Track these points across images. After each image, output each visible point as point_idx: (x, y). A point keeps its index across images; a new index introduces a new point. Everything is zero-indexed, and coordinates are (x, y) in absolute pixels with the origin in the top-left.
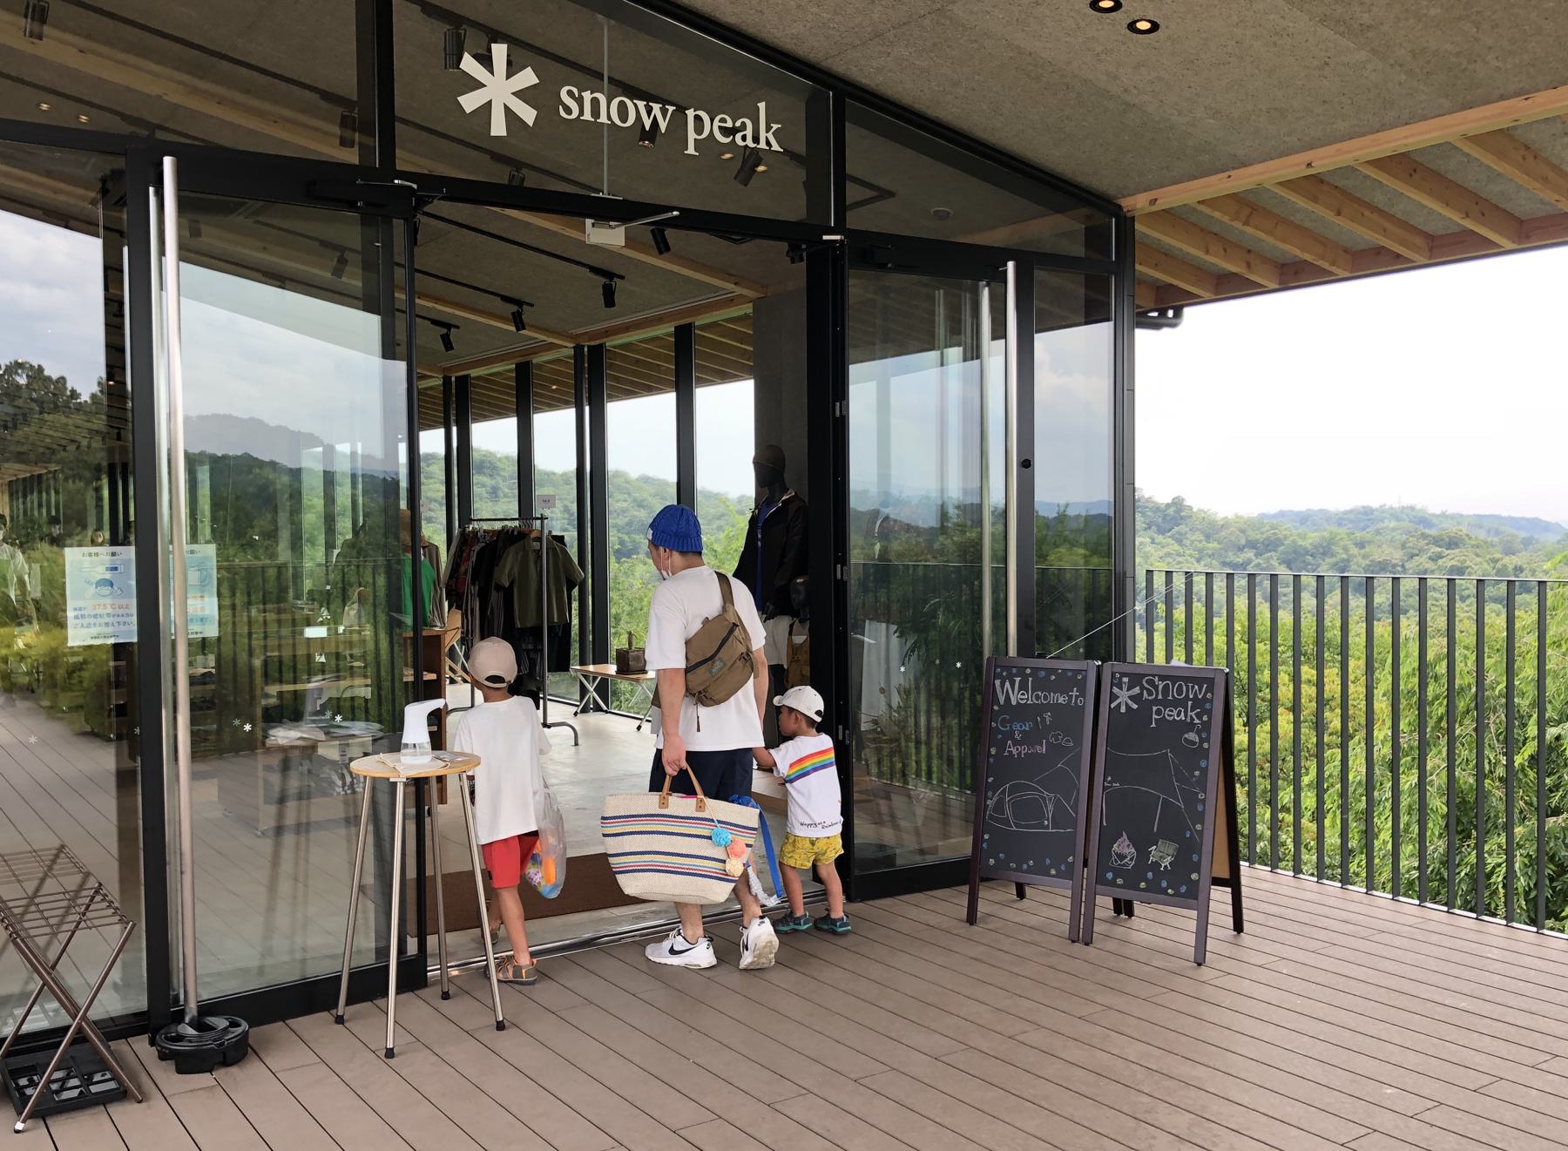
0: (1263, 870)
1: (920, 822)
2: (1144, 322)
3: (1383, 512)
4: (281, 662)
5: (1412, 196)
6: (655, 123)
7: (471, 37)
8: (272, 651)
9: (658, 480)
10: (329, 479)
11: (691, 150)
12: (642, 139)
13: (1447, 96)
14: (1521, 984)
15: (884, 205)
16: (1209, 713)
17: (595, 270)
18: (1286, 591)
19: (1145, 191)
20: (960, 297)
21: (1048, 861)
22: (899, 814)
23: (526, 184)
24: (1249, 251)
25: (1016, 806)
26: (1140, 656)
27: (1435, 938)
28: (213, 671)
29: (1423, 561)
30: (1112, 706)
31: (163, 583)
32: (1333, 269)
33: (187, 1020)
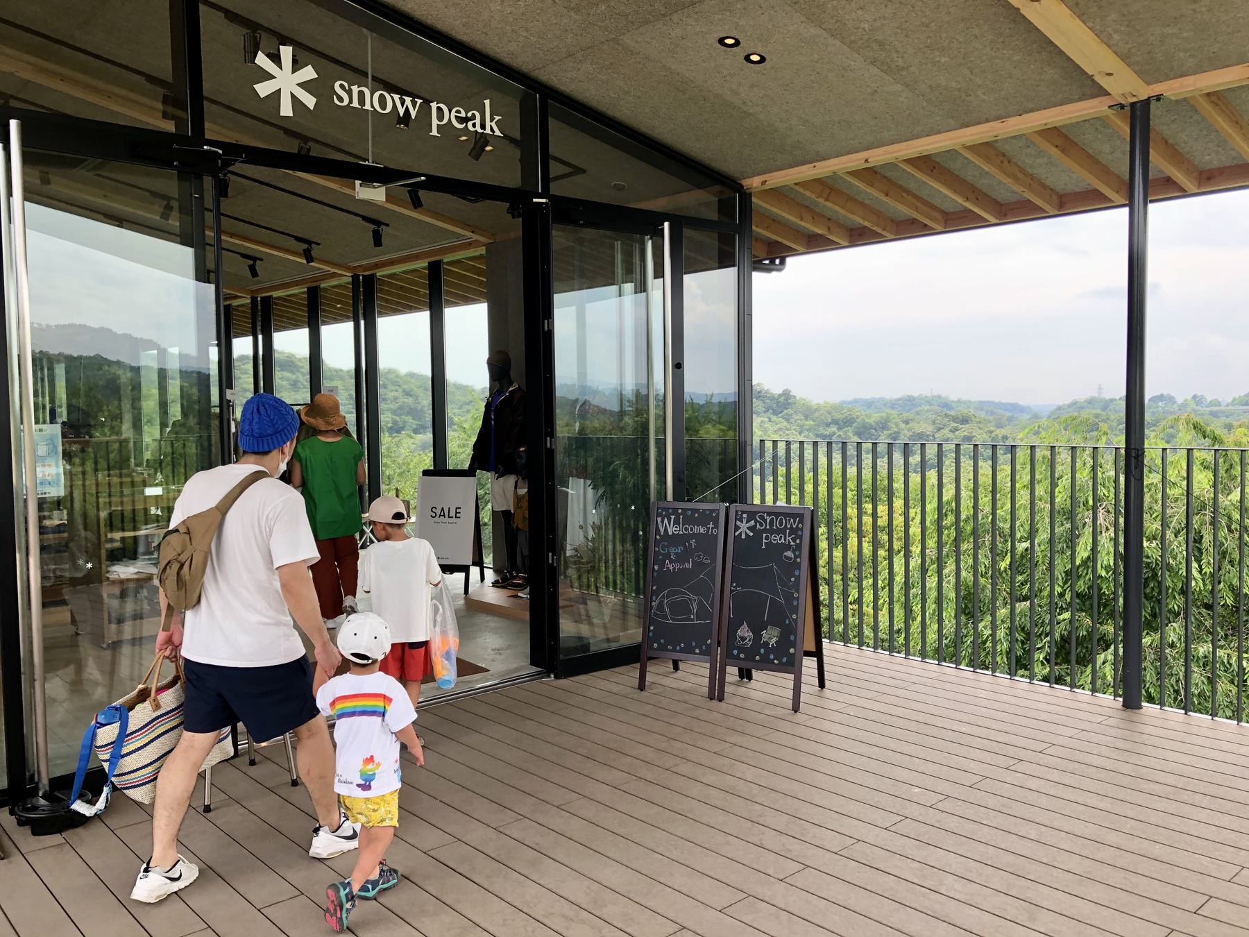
0: (839, 645)
1: (607, 619)
2: (758, 266)
3: (921, 399)
4: (122, 514)
5: (933, 185)
6: (407, 110)
7: (265, 39)
8: (117, 506)
9: (422, 375)
10: (162, 374)
11: (434, 132)
12: (399, 123)
13: (953, 117)
14: (1000, 713)
15: (578, 179)
16: (801, 538)
17: (367, 219)
18: (852, 451)
19: (759, 175)
20: (632, 246)
21: (694, 644)
22: (592, 614)
23: (311, 154)
24: (829, 219)
25: (672, 606)
26: (757, 501)
27: (948, 686)
28: (66, 522)
29: (946, 433)
30: (737, 534)
31: (16, 454)
32: (884, 233)
33: (41, 794)
